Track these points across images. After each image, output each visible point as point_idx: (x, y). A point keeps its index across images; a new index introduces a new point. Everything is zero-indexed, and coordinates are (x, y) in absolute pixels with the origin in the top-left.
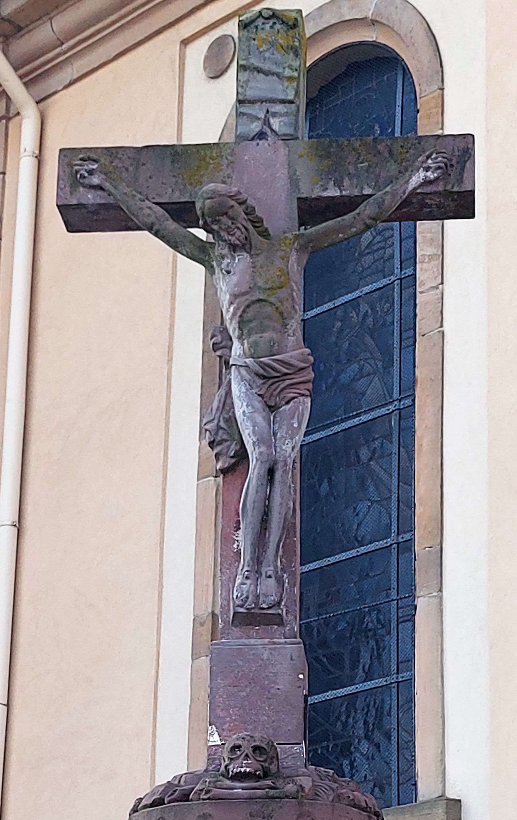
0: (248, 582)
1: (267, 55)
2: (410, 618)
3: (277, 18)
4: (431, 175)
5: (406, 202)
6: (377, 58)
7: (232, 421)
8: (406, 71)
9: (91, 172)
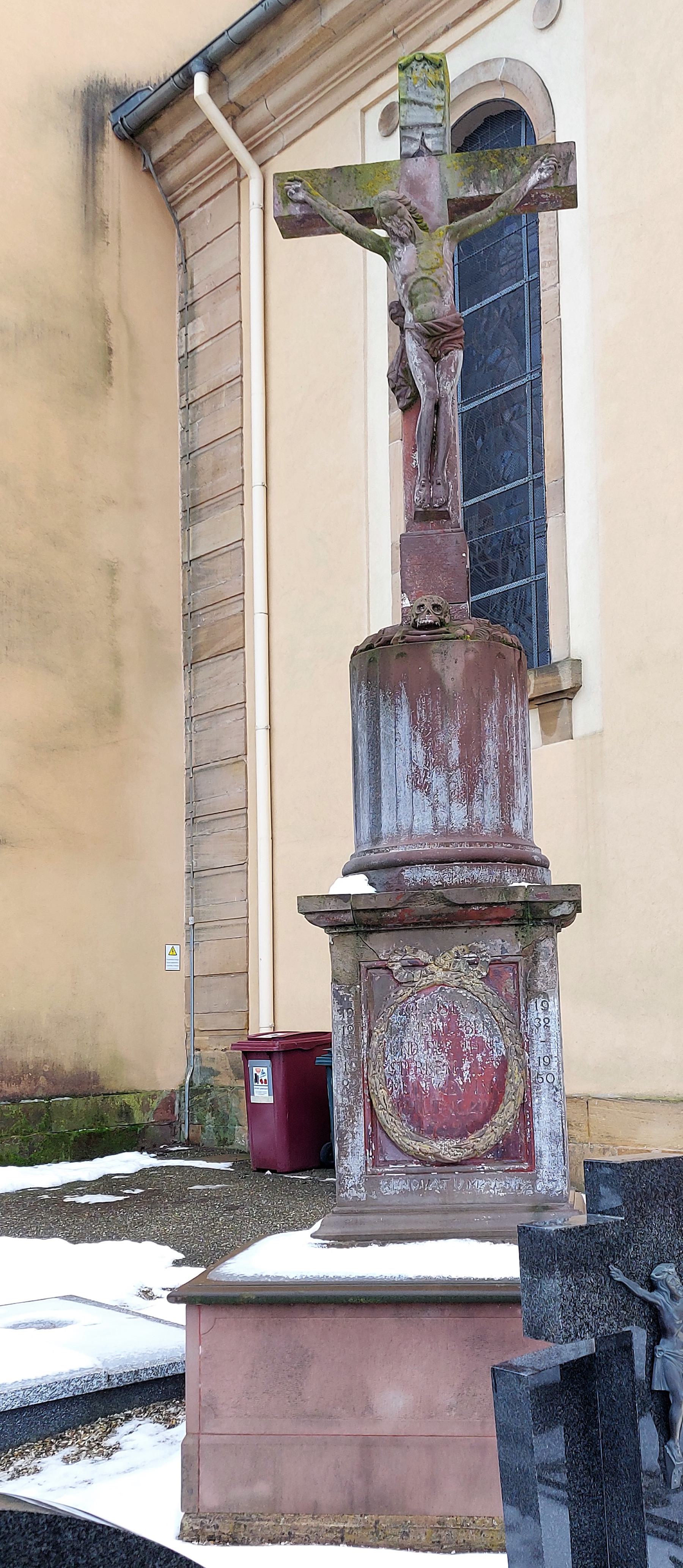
0: (424, 489)
1: (421, 89)
2: (542, 535)
3: (427, 60)
4: (544, 175)
5: (527, 198)
6: (506, 112)
7: (407, 371)
8: (528, 121)
9: (297, 190)
